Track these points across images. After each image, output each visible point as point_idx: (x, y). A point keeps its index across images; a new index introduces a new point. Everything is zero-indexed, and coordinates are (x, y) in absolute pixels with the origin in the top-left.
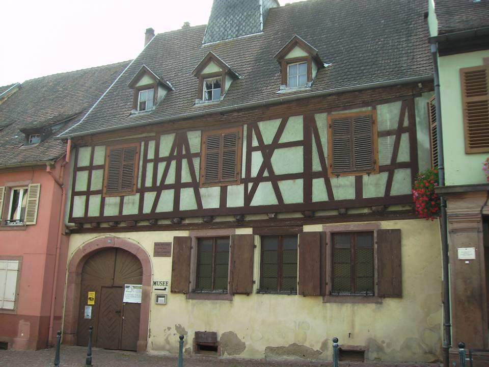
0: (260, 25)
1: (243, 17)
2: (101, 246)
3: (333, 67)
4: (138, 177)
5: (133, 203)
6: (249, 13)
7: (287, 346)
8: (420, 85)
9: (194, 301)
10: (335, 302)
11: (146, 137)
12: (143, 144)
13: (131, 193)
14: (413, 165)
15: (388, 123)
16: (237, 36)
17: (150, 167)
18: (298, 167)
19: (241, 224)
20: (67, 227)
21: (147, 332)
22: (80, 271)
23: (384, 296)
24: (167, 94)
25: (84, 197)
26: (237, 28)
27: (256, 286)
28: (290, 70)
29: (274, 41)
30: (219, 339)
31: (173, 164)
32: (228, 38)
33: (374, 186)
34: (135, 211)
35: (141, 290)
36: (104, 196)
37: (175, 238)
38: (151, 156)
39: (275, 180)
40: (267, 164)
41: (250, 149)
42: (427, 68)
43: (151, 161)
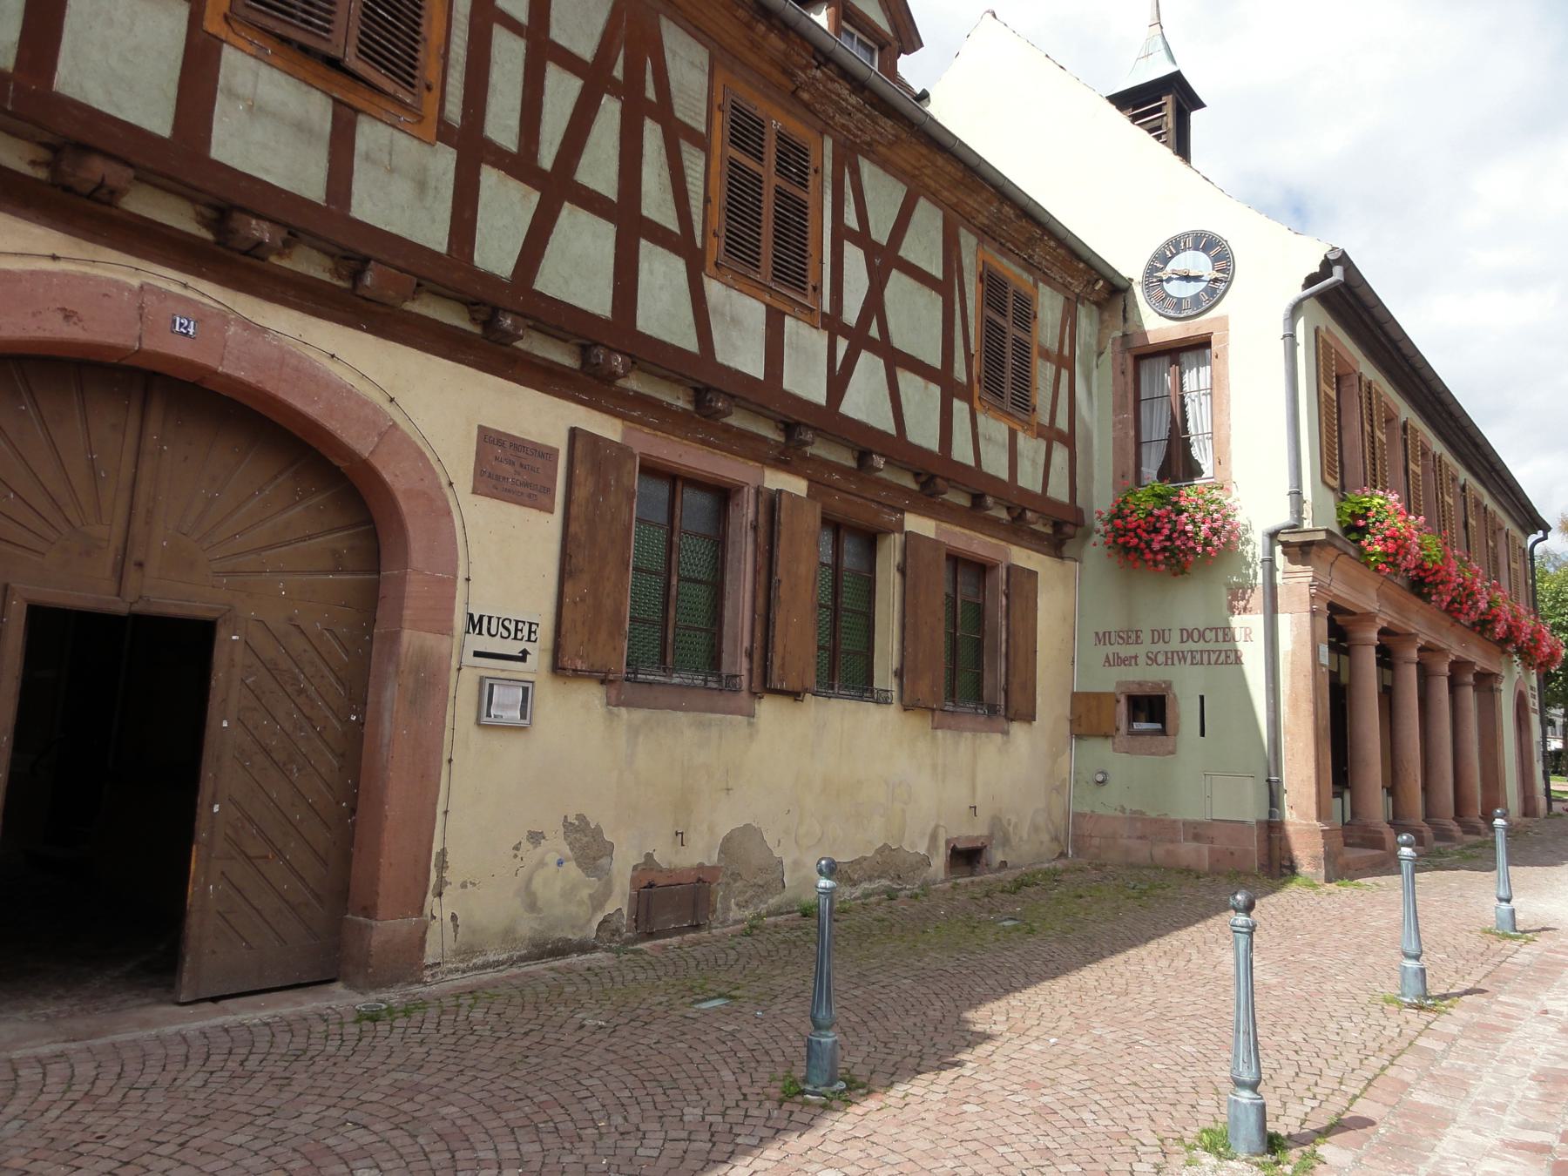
5: (422, 186)
9: (639, 715)
41: (841, 234)
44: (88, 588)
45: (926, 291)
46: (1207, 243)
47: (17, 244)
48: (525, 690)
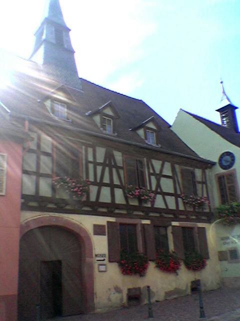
21: (93, 294)
41: (150, 174)
45: (169, 179)
46: (229, 154)
47: (35, 215)
48: (105, 271)
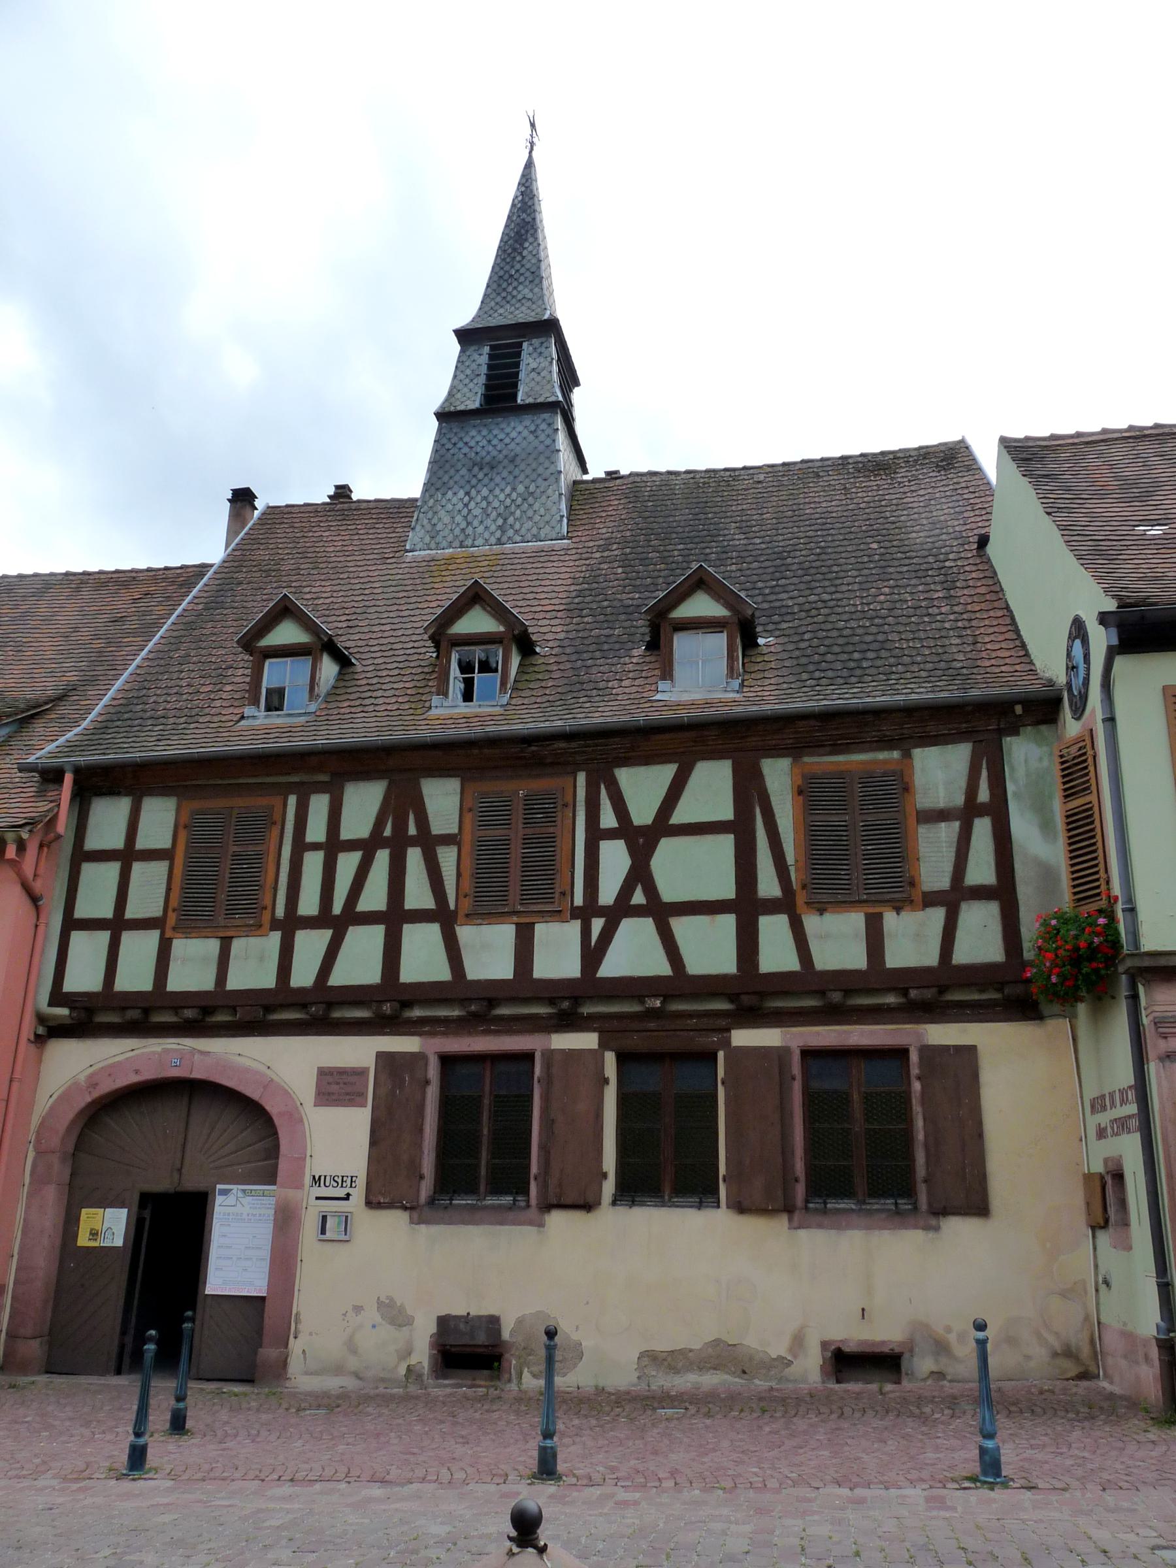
0: (561, 521)
1: (514, 495)
2: (148, 1074)
3: (779, 648)
4: (275, 889)
5: (261, 959)
6: (532, 489)
7: (698, 1347)
8: (1019, 709)
10: (820, 1226)
11: (302, 783)
12: (292, 800)
13: (256, 929)
14: (1003, 892)
15: (942, 793)
16: (499, 542)
17: (313, 863)
18: (721, 884)
19: (568, 1021)
20: (41, 1019)
22: (70, 1148)
23: (942, 1211)
24: (340, 673)
25: (104, 936)
26: (500, 522)
27: (609, 1187)
28: (683, 645)
29: (605, 566)
30: (506, 1335)
31: (382, 858)
32: (476, 543)
33: (912, 941)
34: (267, 980)
35: (272, 1201)
36: (167, 936)
37: (381, 1056)
38: (316, 831)
39: (662, 913)
40: (640, 874)
41: (595, 835)
42: (1018, 667)
43: (315, 846)
44: (162, 1184)
